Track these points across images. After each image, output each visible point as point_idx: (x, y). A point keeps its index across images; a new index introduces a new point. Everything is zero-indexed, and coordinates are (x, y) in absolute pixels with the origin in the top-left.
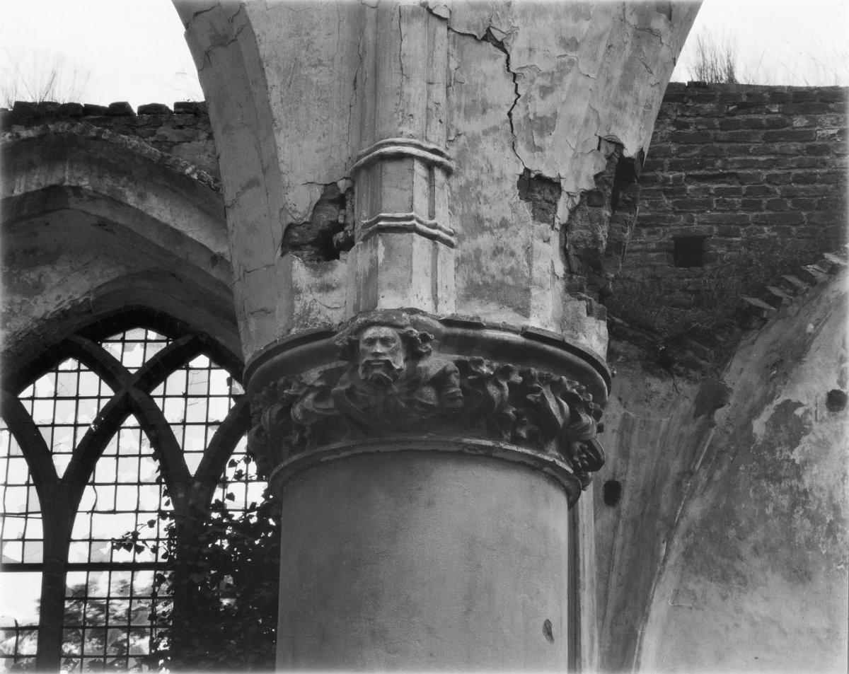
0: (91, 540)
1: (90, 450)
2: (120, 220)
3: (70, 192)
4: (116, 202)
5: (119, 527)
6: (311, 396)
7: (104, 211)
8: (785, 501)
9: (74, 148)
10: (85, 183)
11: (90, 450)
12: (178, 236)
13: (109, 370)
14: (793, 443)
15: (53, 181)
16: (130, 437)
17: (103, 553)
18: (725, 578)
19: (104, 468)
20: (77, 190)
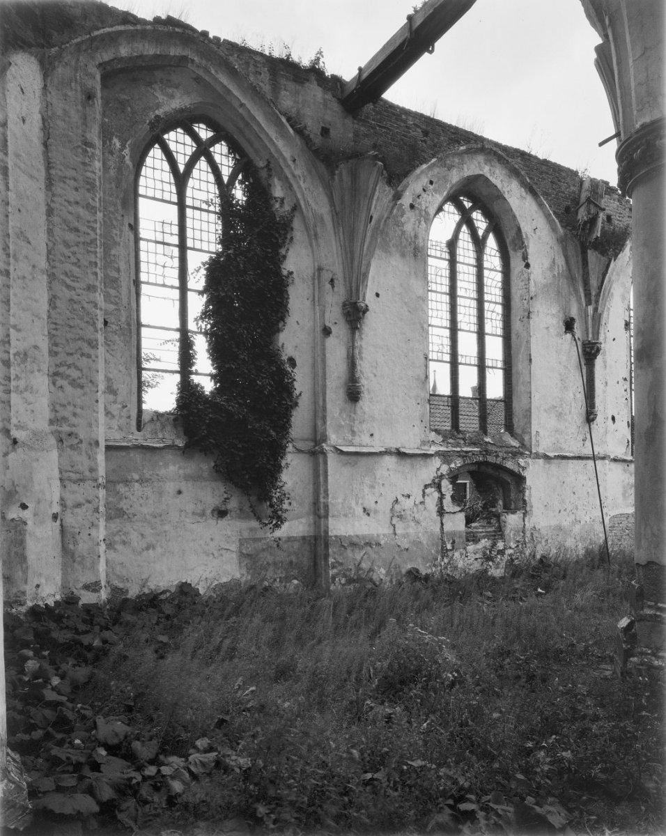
0: (193, 198)
1: (190, 165)
2: (207, 78)
3: (190, 61)
4: (207, 71)
5: (204, 196)
6: (48, 713)
7: (201, 73)
8: (400, 233)
9: (234, 202)
10: (354, 676)
11: (190, 165)
12: (229, 91)
13: (195, 137)
14: (402, 216)
15: (184, 54)
16: (202, 164)
17: (197, 204)
18: (386, 252)
19: (195, 173)
20: (193, 61)
